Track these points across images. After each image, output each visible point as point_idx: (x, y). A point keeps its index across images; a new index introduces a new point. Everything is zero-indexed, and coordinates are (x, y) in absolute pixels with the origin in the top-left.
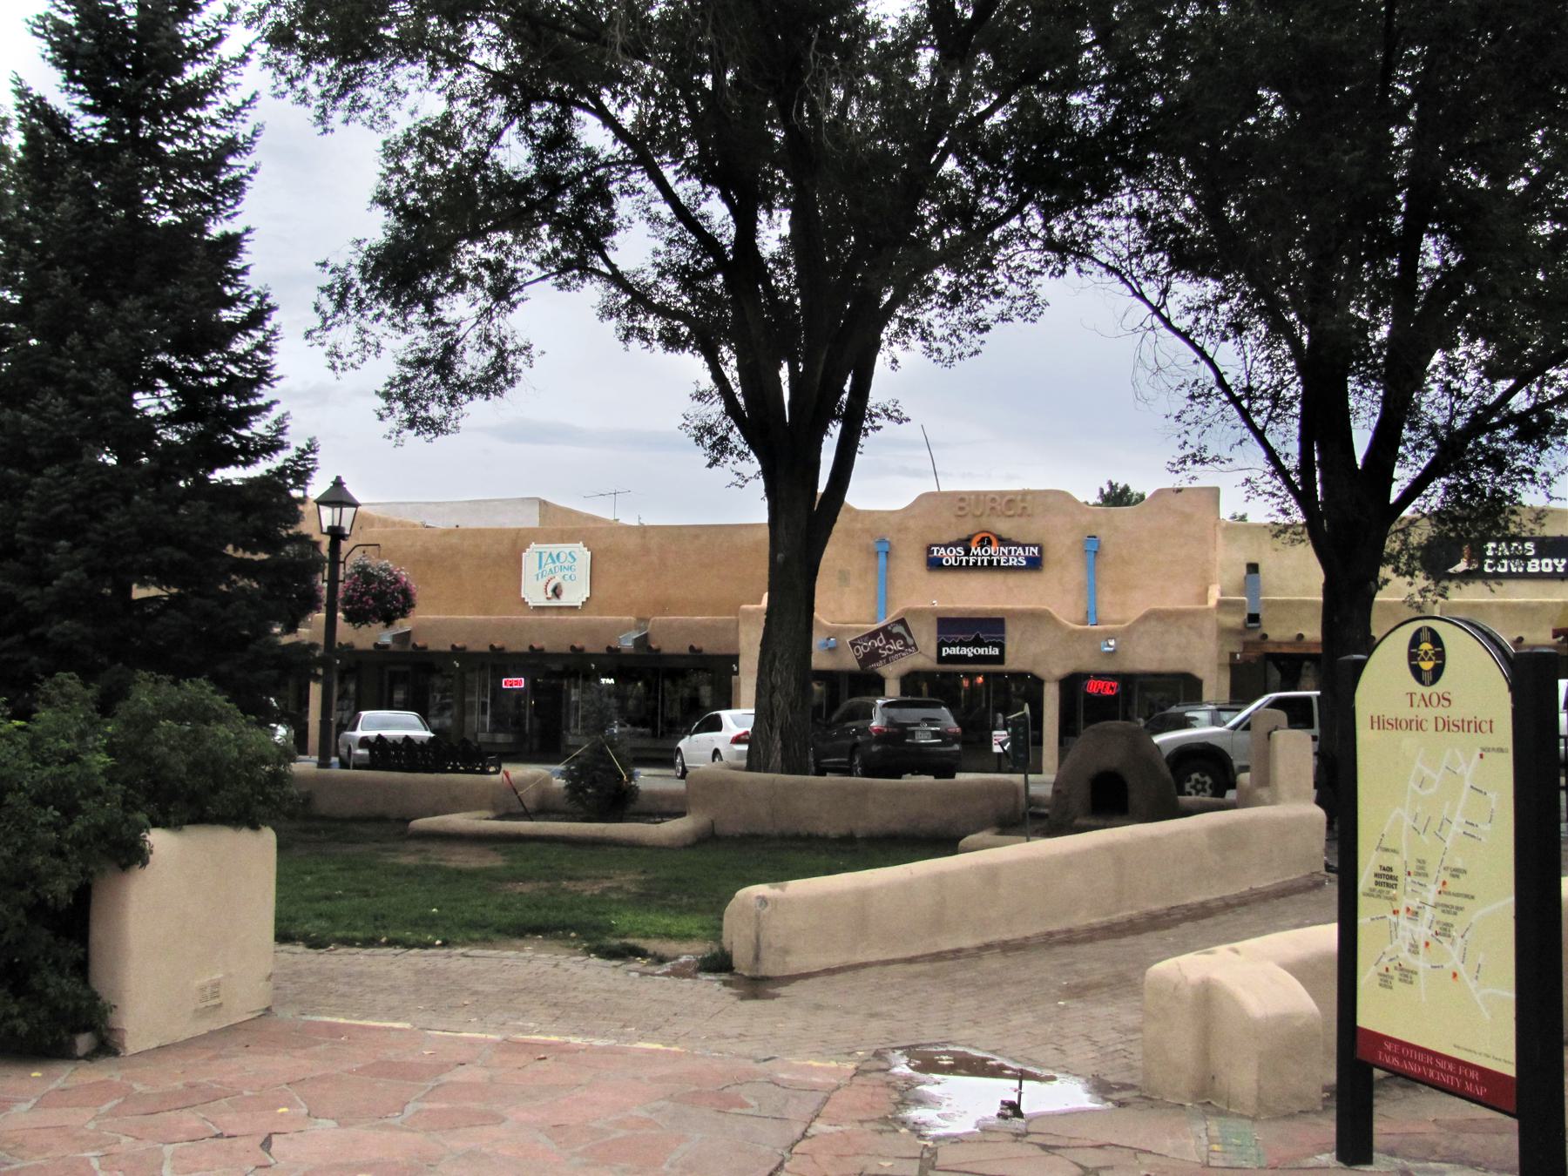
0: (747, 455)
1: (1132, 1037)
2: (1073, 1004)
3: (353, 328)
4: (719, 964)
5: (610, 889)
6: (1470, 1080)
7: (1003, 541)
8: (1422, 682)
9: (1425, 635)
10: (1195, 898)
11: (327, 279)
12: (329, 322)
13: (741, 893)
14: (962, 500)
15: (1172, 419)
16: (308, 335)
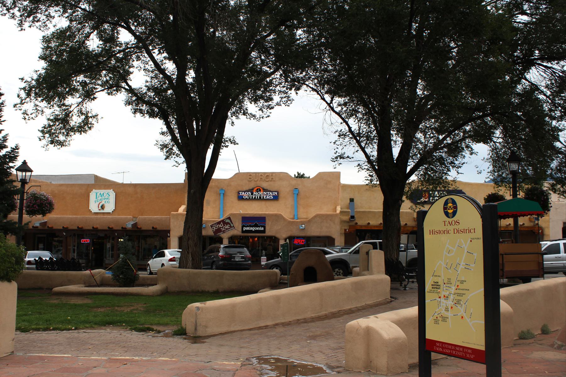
0: (179, 155)
1: (337, 351)
2: (312, 341)
3: (32, 104)
4: (181, 333)
5: (134, 309)
6: (468, 353)
7: (265, 190)
8: (449, 217)
9: (450, 201)
10: (347, 307)
11: (23, 85)
12: (24, 101)
13: (189, 306)
14: (250, 175)
15: (332, 143)
16: (15, 106)
